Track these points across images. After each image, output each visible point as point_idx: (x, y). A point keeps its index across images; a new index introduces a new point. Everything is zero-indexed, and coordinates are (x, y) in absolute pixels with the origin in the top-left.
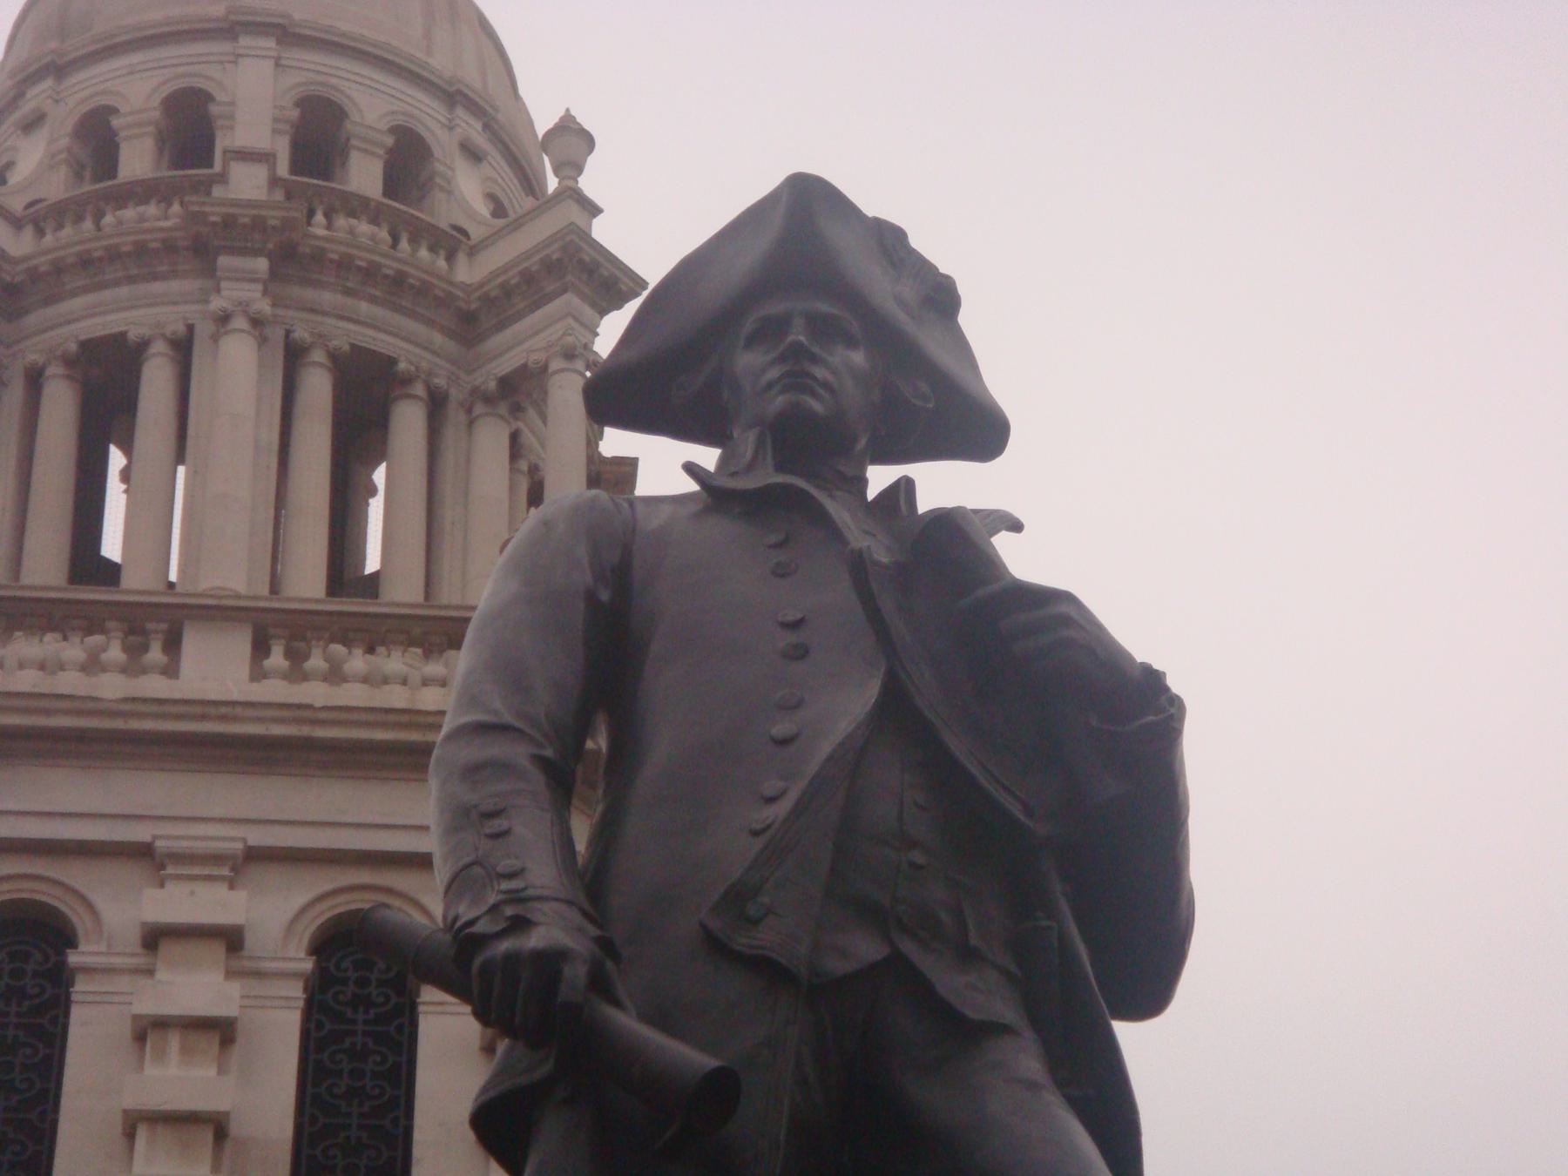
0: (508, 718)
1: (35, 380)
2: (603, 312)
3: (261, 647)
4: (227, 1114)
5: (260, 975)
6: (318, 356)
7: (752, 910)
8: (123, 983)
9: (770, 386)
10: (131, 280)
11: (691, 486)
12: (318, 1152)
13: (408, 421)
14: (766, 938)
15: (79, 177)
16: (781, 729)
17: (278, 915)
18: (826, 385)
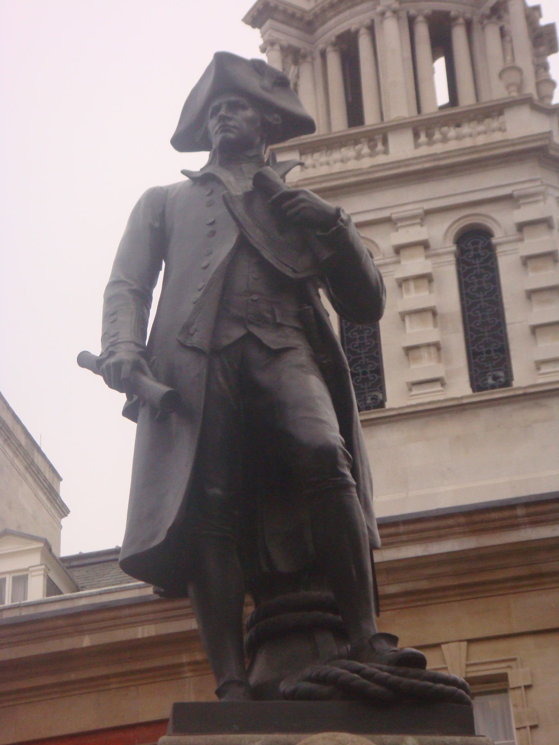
1: (323, 54)
3: (416, 135)
4: (435, 307)
5: (438, 255)
6: (420, 18)
8: (391, 268)
11: (185, 178)
12: (471, 313)
13: (459, 36)
17: (441, 233)
18: (235, 127)
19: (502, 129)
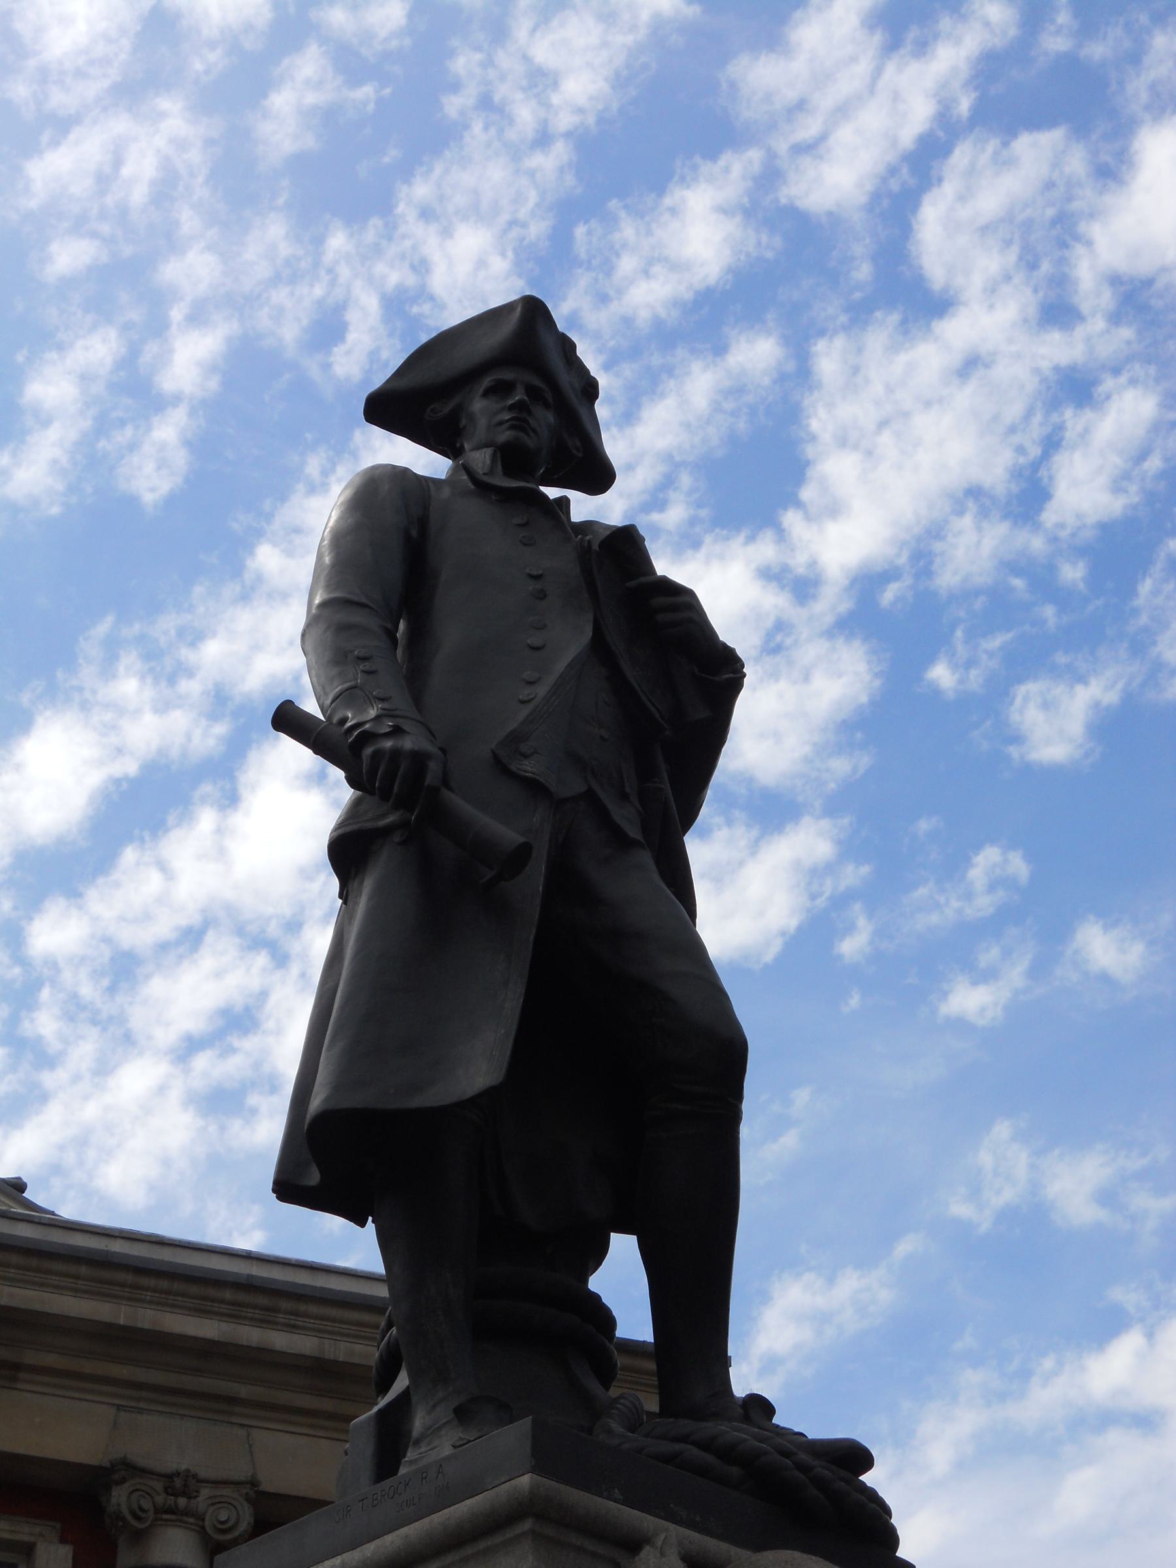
0: (364, 600)
7: (524, 748)
9: (501, 423)
14: (529, 768)
16: (535, 641)
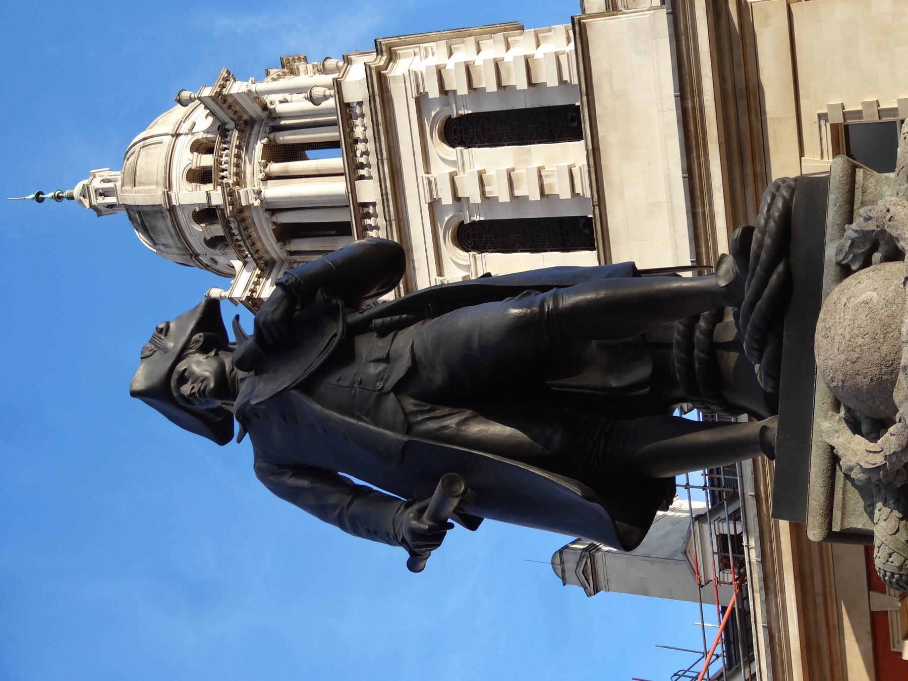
1: (292, 253)
2: (256, 323)
3: (362, 177)
10: (256, 229)
15: (227, 246)
17: (440, 150)
19: (360, 104)
